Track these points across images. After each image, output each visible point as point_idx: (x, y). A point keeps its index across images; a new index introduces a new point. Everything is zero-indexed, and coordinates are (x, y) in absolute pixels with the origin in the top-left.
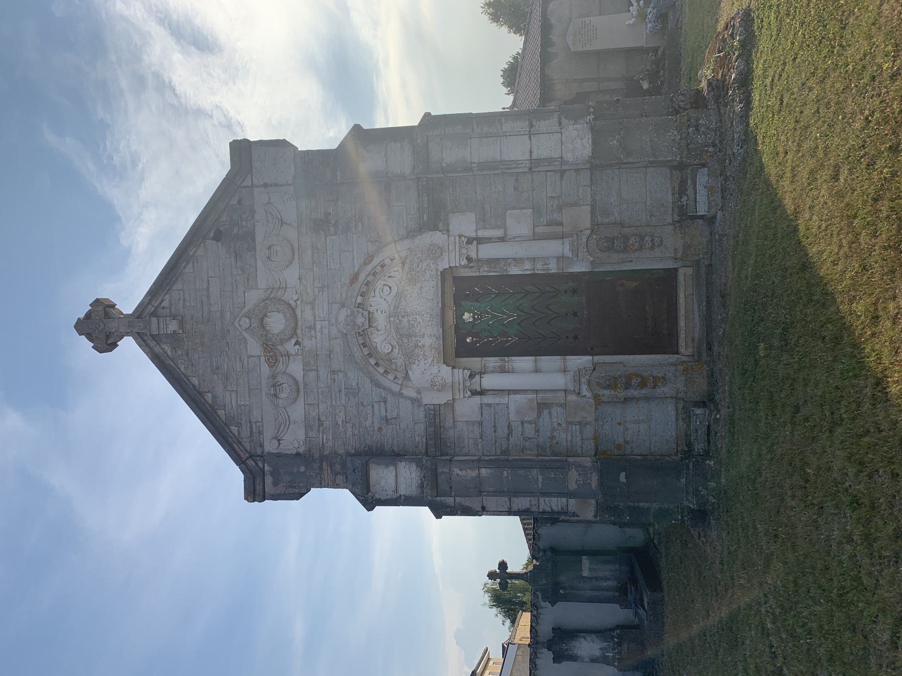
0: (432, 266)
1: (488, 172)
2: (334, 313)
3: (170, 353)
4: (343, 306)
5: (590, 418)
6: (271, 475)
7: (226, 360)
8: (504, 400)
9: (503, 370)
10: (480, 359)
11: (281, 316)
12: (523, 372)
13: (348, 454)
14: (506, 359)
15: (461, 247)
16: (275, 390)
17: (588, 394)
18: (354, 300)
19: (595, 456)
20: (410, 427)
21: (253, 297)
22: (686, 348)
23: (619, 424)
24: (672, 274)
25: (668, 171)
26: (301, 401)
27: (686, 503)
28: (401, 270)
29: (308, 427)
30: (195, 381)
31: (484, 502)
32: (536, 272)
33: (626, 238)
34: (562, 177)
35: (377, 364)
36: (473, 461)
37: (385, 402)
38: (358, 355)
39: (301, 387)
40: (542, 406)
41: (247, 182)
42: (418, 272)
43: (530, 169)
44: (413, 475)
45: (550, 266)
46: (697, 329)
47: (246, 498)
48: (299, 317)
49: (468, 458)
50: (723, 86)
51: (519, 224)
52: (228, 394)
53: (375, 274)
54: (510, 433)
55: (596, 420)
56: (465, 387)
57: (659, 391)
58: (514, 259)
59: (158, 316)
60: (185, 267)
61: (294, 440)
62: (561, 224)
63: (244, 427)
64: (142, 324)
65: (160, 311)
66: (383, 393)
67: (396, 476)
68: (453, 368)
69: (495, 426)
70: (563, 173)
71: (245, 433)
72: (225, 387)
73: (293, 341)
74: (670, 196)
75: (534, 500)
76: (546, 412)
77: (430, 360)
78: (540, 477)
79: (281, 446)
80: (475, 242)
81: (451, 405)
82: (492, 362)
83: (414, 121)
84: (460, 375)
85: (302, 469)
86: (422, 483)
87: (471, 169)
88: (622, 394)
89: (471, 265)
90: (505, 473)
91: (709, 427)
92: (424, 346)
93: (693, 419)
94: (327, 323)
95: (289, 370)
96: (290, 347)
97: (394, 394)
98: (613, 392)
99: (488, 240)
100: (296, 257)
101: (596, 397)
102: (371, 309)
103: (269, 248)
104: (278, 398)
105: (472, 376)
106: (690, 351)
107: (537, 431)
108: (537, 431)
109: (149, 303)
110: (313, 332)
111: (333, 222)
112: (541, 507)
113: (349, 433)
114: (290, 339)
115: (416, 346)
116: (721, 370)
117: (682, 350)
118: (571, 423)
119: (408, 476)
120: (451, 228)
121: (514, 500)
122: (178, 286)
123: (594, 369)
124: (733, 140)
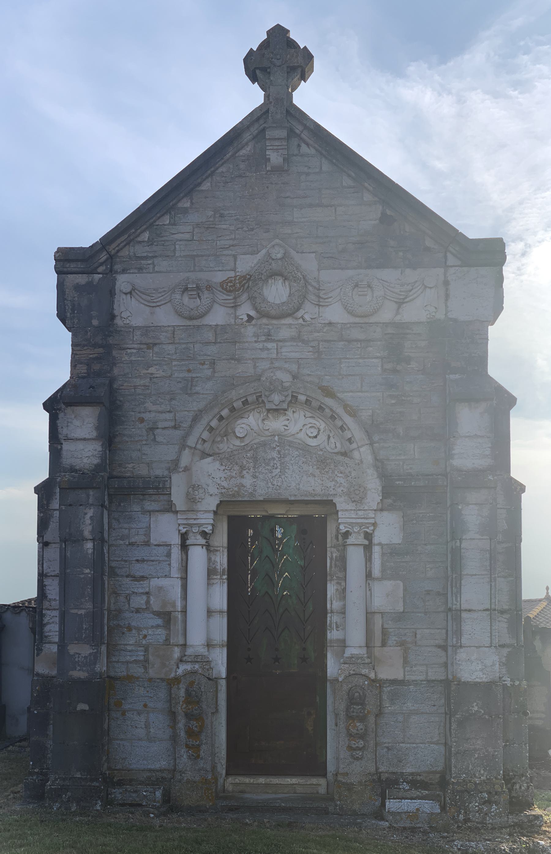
0: (339, 490)
1: (449, 559)
2: (286, 366)
3: (242, 152)
4: (295, 377)
5: (152, 673)
6: (88, 280)
7: (232, 228)
8: (175, 573)
9: (211, 572)
10: (226, 545)
11: (285, 299)
12: (208, 595)
13: (112, 381)
14: (225, 577)
15: (361, 525)
16: (192, 290)
17: (180, 671)
18: (301, 391)
19: (109, 677)
20: (148, 456)
21: (308, 264)
22: (231, 783)
23: (145, 706)
24: (315, 766)
25: (440, 769)
26: (176, 321)
27: (52, 777)
28: (336, 451)
29: (146, 330)
30: (206, 186)
31: (54, 545)
32: (329, 615)
33: (363, 719)
34: (439, 647)
35: (221, 418)
36: (102, 532)
37: (175, 427)
38: (233, 394)
39: (196, 322)
40: (167, 617)
41: (451, 260)
42: (333, 472)
43: (450, 610)
44: (85, 460)
45: (335, 632)
46: (254, 797)
47: (60, 250)
48: (283, 321)
49: (106, 527)
50: (532, 832)
51: (386, 595)
52: (189, 228)
53: (333, 418)
54: (136, 579)
55: (150, 680)
56: (191, 525)
57: (183, 751)
58: (344, 590)
59: (288, 138)
60: (349, 176)
61: (131, 312)
62: (384, 644)
63: (147, 249)
64: (279, 116)
65: (295, 141)
66: (185, 425)
67: (85, 439)
68: (215, 513)
69: (143, 561)
70: (444, 648)
71: (140, 250)
72: (198, 225)
73: (253, 313)
74: (409, 770)
75: (55, 604)
76: (159, 621)
77: (225, 484)
78: (82, 612)
79: (124, 296)
80: (366, 542)
81: (170, 508)
82: (222, 560)
83: (517, 472)
84: (206, 520)
85: (95, 322)
86: (76, 471)
87: (453, 539)
88: (180, 709)
89: (340, 537)
90: (87, 571)
91: (140, 805)
92: (243, 477)
93: (150, 789)
94: (274, 356)
95: (216, 306)
96: (246, 310)
97: (185, 438)
98: (182, 699)
99: (369, 559)
100: (357, 320)
101: (177, 680)
102: (290, 413)
103: (369, 286)
104: (183, 292)
105: (204, 534)
106: (229, 787)
107: (138, 611)
108: (138, 611)
109: (306, 127)
110: (263, 338)
111: (399, 368)
112: (48, 612)
113: (138, 382)
114: (256, 309)
115: (242, 468)
116: (206, 820)
117: (230, 779)
118: (146, 650)
119: (85, 453)
120: (385, 513)
121: (56, 581)
122: (326, 166)
123: (209, 679)
124: (469, 841)
